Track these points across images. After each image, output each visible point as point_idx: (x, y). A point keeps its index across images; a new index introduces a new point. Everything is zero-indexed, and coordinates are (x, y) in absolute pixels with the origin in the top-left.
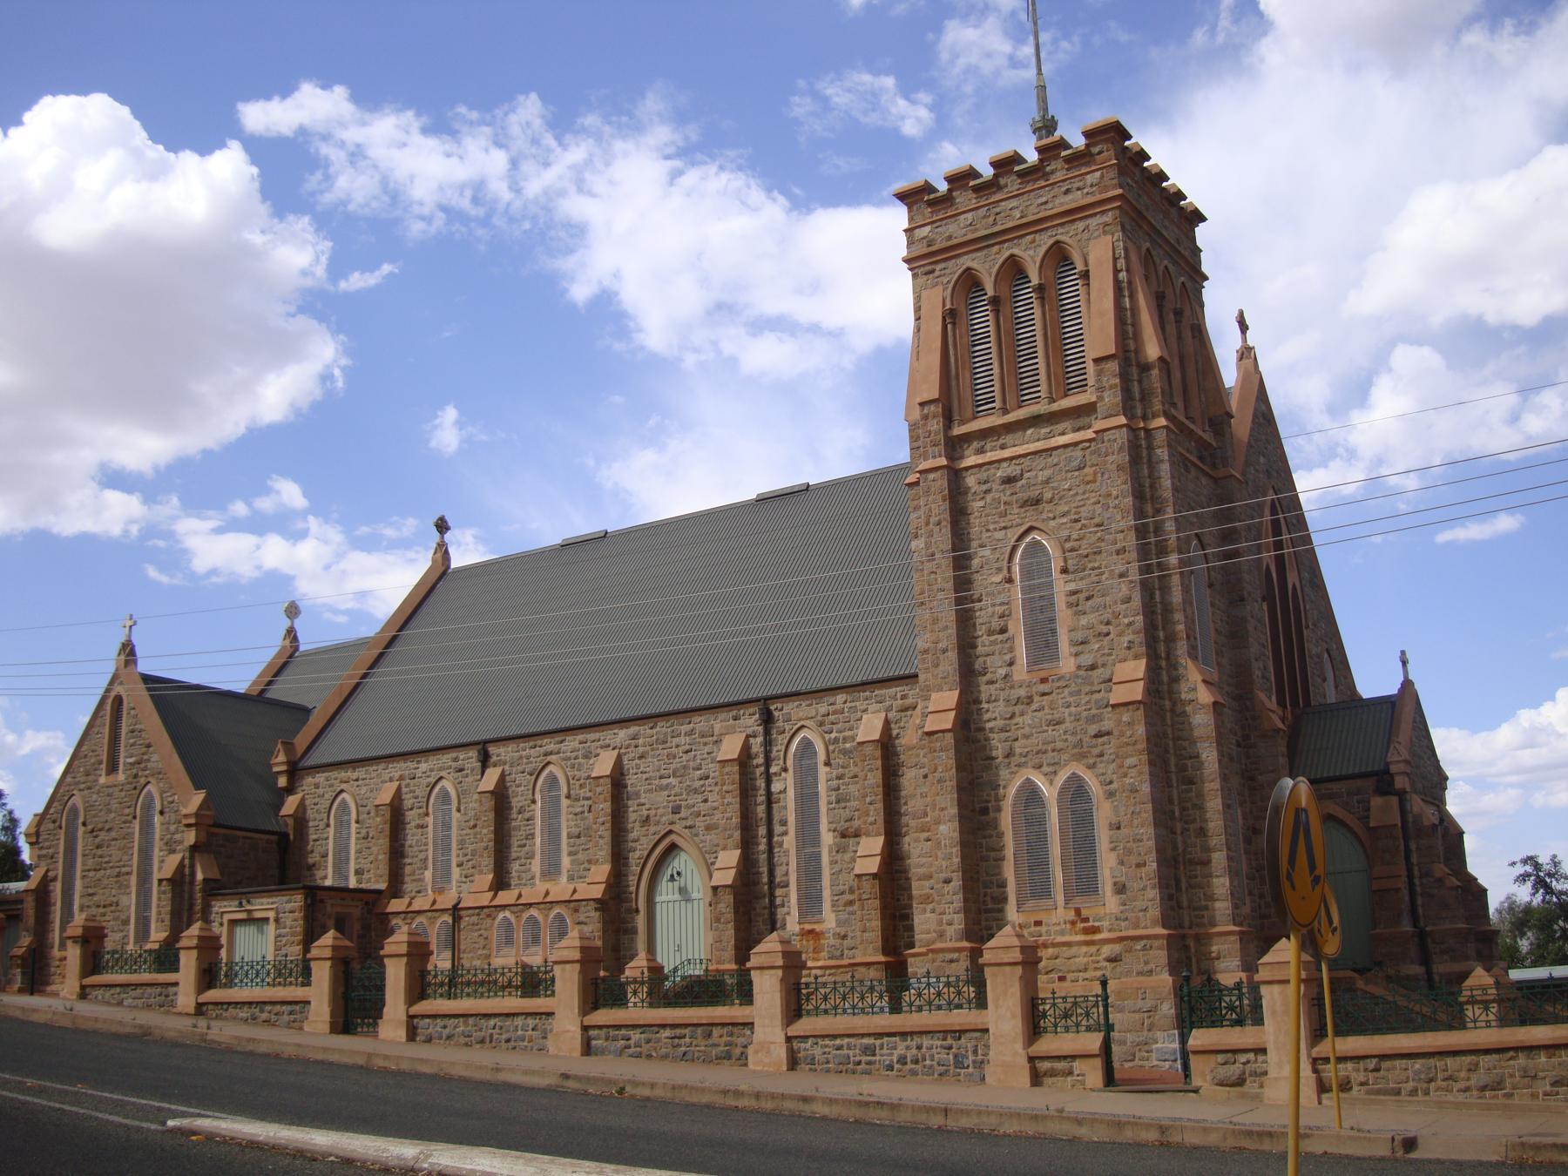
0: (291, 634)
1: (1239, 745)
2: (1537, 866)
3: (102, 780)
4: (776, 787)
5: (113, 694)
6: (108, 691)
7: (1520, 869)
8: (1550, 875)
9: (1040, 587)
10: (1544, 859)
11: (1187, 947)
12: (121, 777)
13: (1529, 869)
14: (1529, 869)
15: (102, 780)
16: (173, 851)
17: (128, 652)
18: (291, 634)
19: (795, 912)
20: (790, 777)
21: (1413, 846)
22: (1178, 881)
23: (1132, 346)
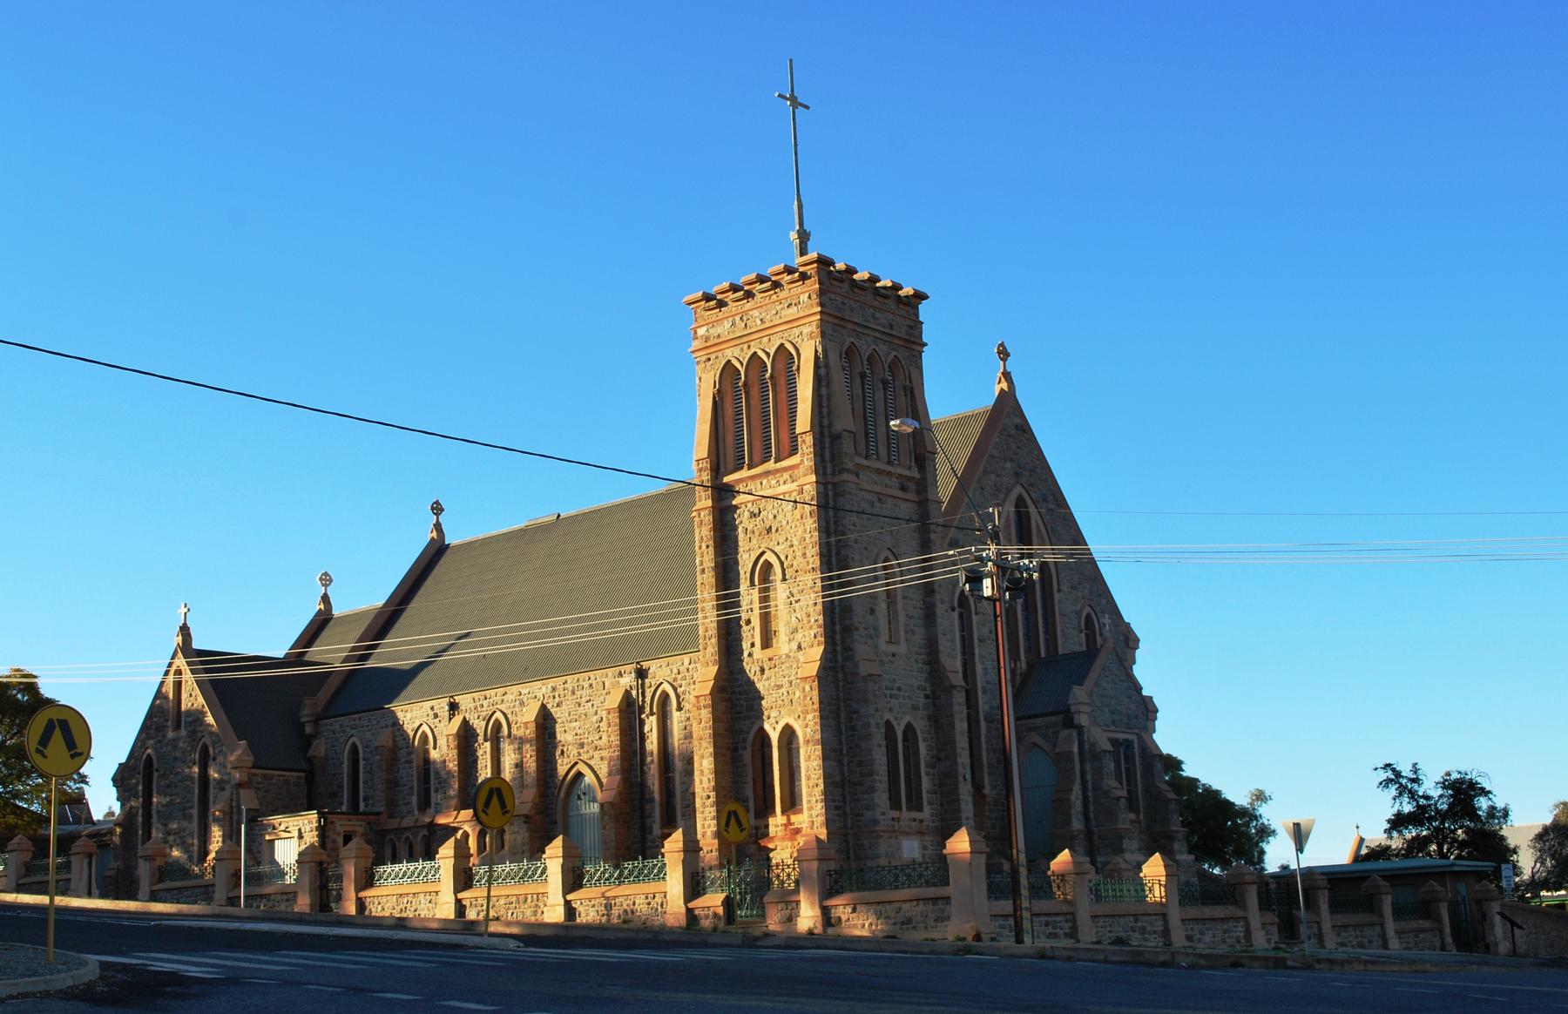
0: (325, 598)
1: (927, 697)
2: (1398, 774)
3: (170, 734)
4: (647, 728)
5: (174, 668)
6: (170, 665)
7: (1383, 775)
8: (1414, 781)
9: (725, 606)
10: (1406, 771)
11: (847, 842)
12: (183, 732)
13: (1390, 775)
14: (1390, 775)
15: (170, 734)
16: (223, 789)
17: (185, 630)
18: (325, 598)
19: (658, 821)
20: (654, 719)
21: (1088, 767)
22: (844, 796)
23: (826, 423)
